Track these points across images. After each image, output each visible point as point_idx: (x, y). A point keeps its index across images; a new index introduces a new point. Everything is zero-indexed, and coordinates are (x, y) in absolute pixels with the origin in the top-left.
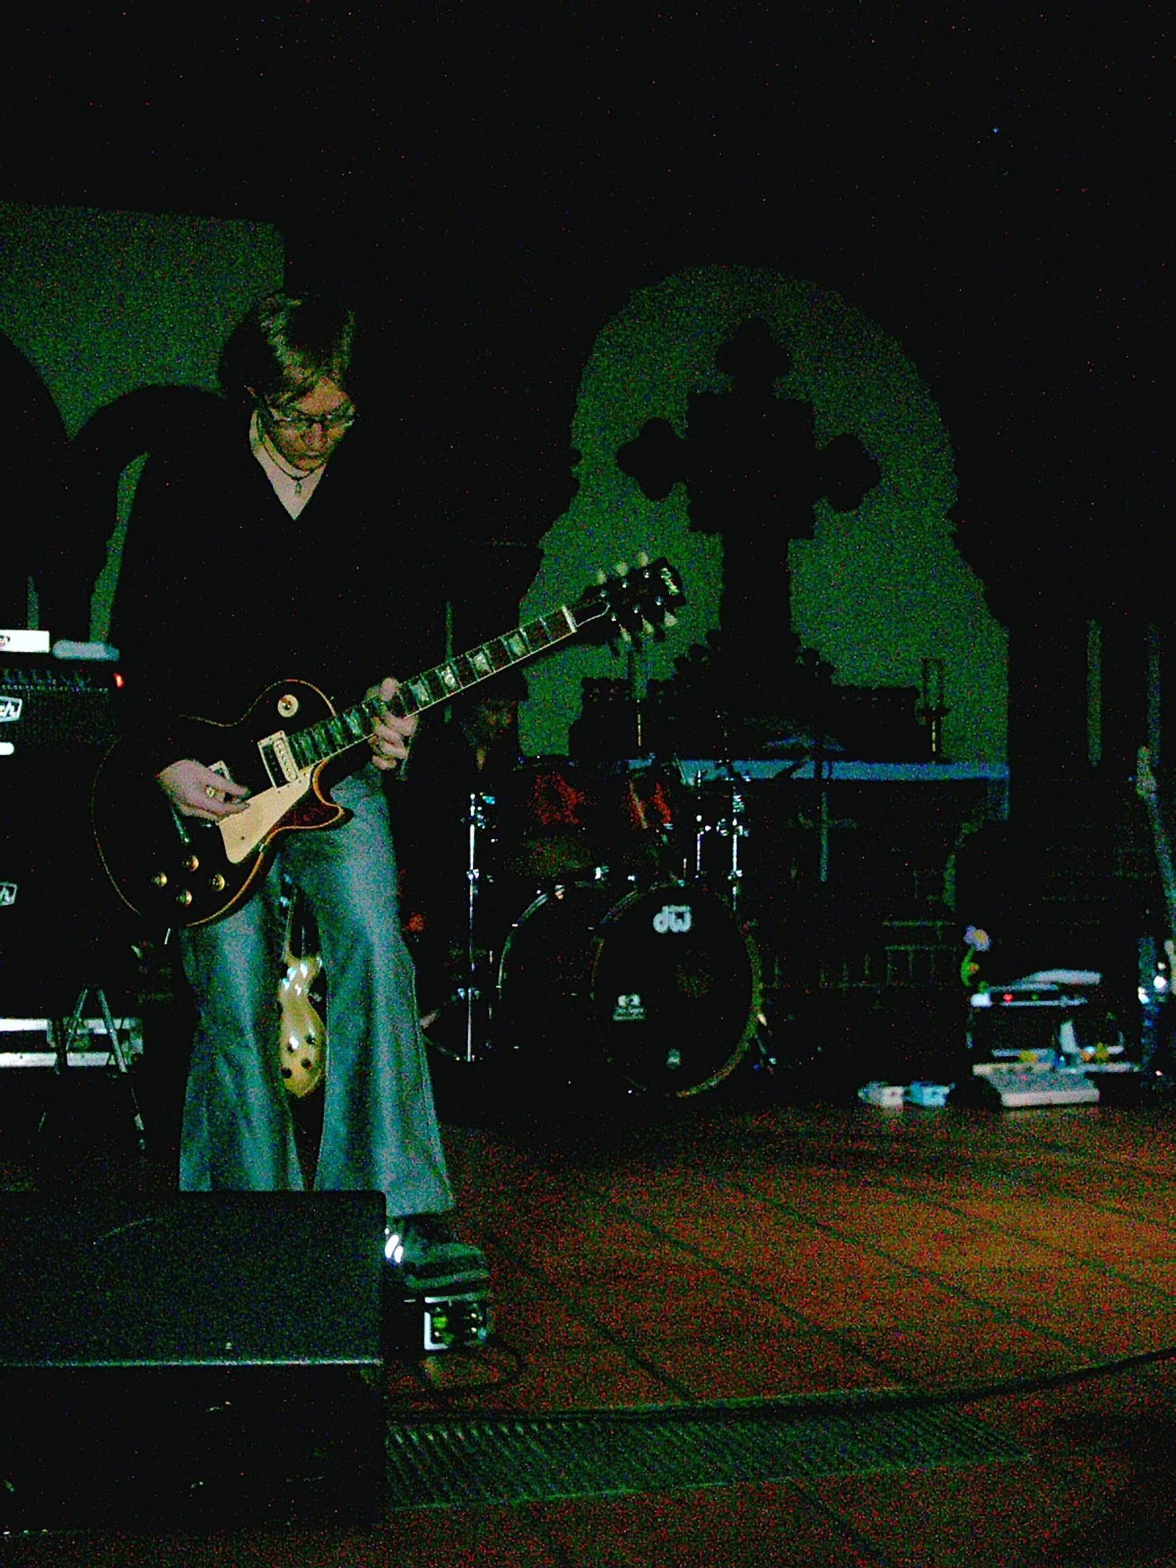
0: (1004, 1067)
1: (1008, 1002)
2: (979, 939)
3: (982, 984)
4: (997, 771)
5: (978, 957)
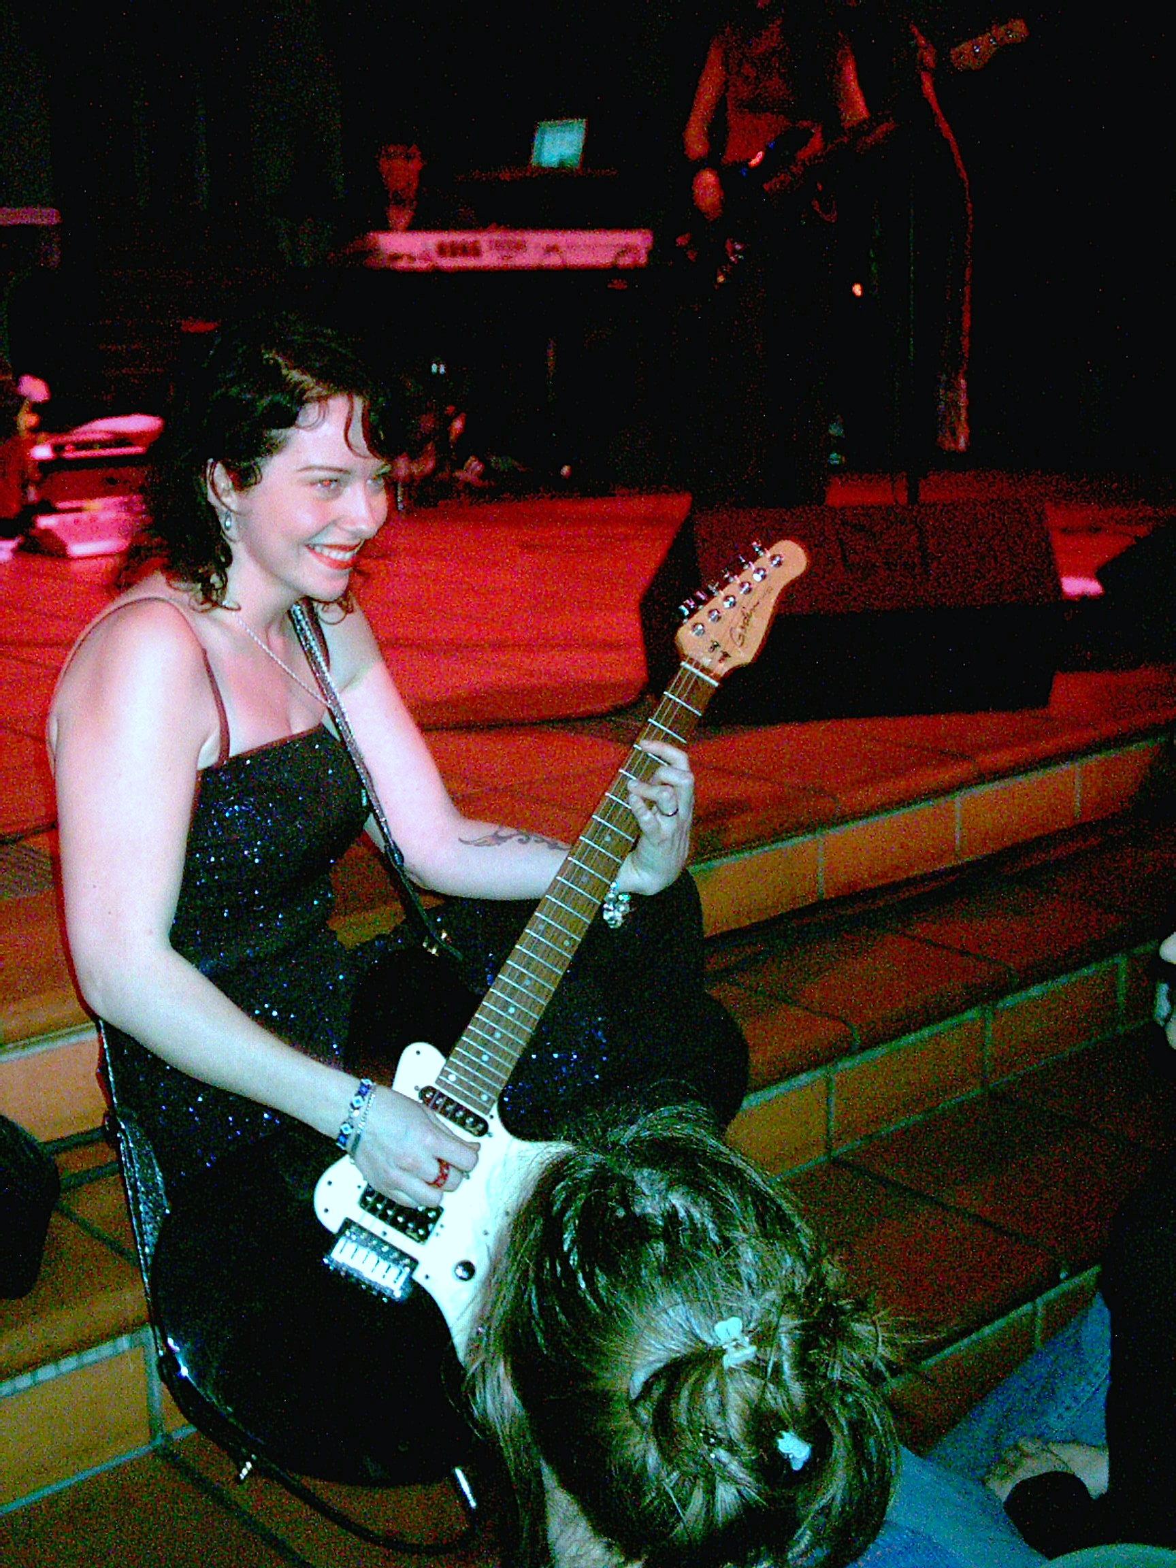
0: (70, 518)
1: (69, 455)
2: (34, 389)
5: (35, 408)
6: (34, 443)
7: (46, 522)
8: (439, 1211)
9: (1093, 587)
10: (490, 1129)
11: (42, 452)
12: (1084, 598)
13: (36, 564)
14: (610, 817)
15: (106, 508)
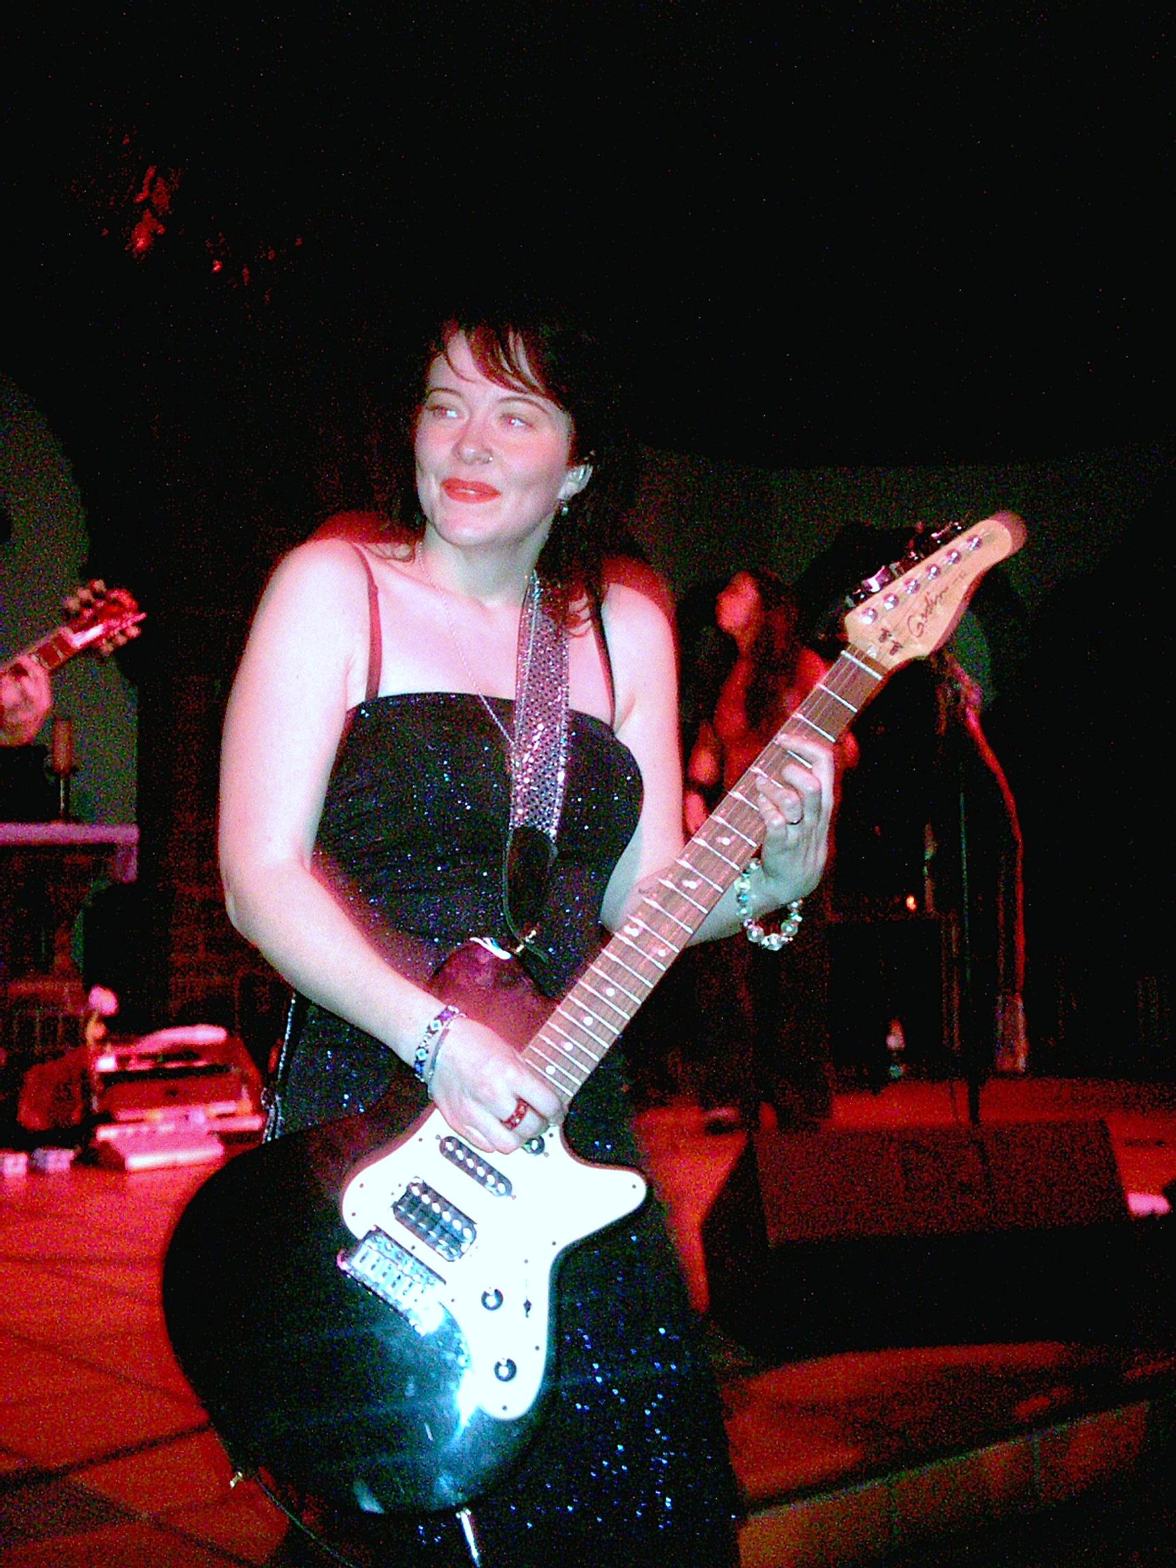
0: (130, 1130)
2: (104, 1000)
3: (108, 1048)
4: (130, 833)
5: (103, 1019)
6: (101, 1053)
7: (106, 1133)
8: (452, 1323)
9: (1159, 1204)
10: (546, 1149)
11: (107, 1064)
12: (1153, 1215)
13: (91, 1178)
14: (733, 816)
15: (166, 1120)
